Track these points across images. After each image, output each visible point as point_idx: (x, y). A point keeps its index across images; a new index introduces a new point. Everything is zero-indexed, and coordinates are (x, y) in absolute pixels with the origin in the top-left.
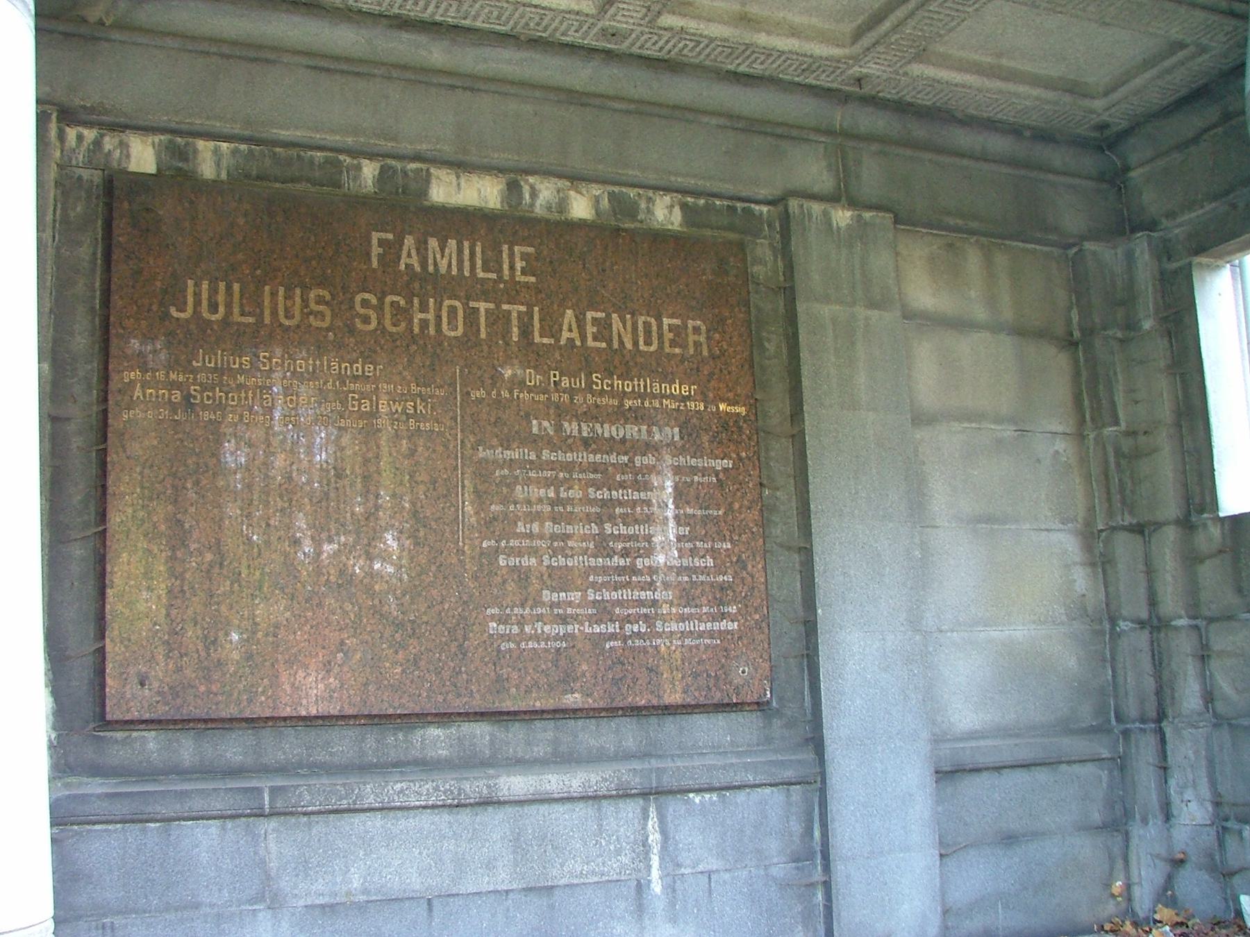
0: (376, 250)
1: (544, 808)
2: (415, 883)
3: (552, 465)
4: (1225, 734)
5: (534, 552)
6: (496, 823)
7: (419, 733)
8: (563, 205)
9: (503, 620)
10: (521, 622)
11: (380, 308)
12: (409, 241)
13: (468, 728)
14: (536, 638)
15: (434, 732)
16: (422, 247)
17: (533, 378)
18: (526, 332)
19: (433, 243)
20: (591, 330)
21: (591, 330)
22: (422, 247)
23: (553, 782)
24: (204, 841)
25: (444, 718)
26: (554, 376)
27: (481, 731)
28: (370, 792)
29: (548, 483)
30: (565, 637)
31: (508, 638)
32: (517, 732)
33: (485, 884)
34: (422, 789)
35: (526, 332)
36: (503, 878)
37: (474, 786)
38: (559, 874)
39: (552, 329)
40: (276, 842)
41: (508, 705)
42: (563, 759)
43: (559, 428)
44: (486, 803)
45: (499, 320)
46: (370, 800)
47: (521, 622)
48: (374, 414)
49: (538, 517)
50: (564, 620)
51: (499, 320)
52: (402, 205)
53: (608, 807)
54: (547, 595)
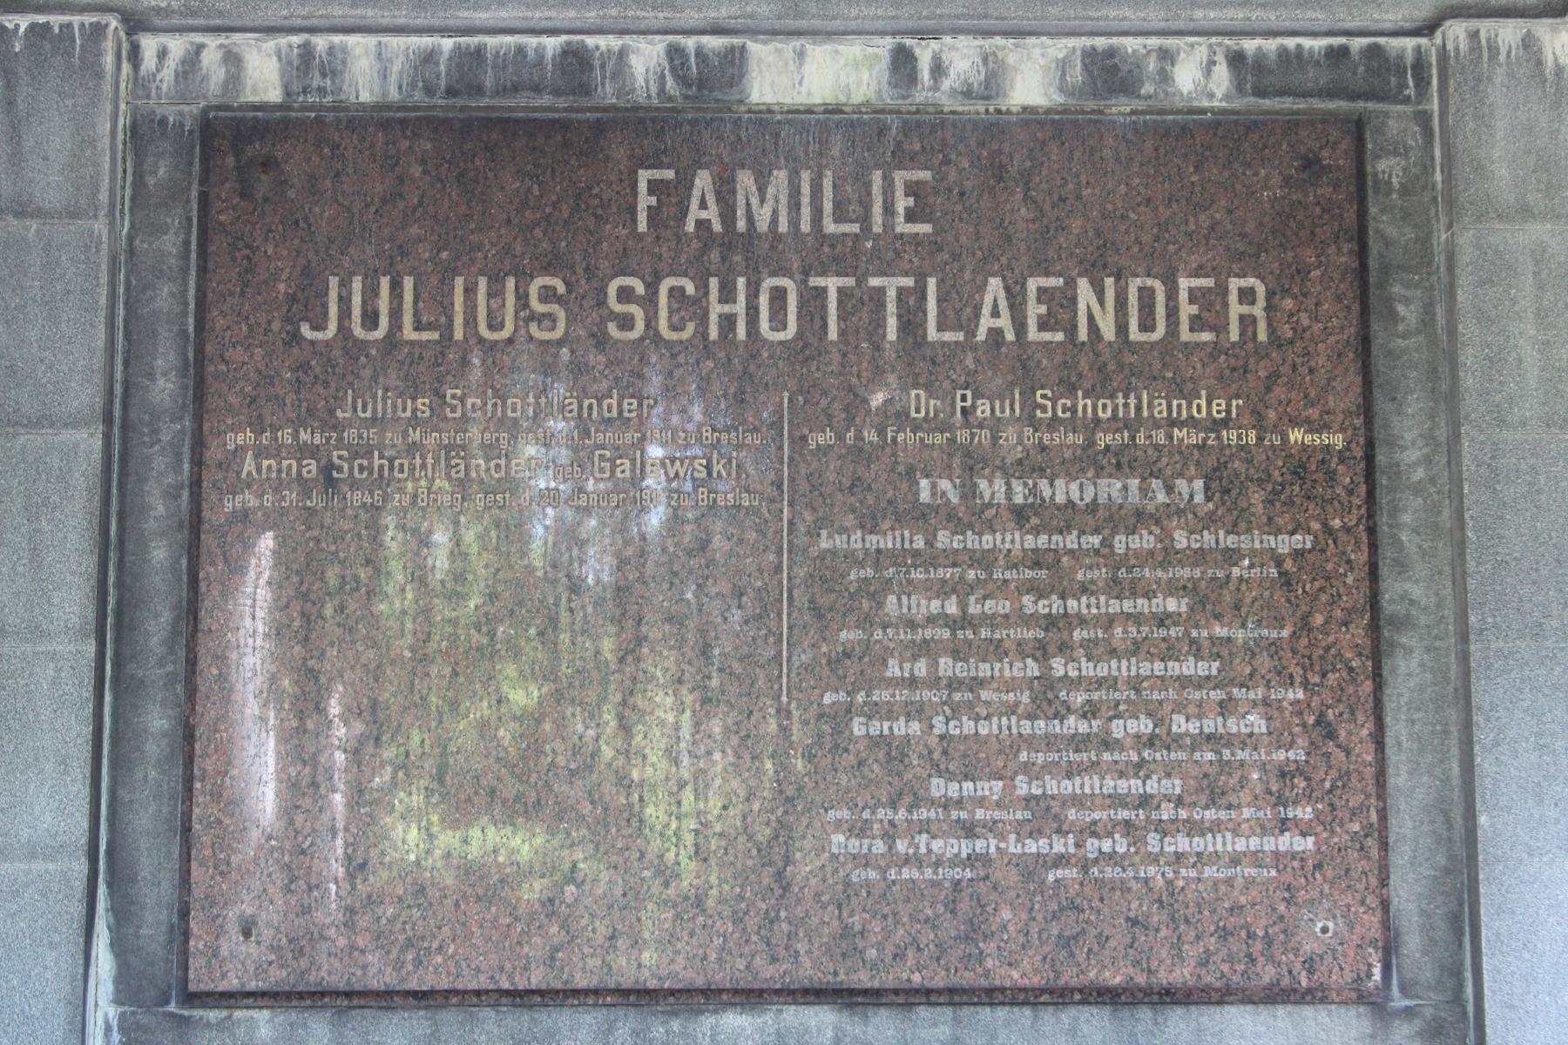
0: (645, 201)
3: (952, 558)
5: (916, 711)
8: (994, 79)
9: (860, 830)
10: (889, 836)
11: (650, 301)
12: (703, 181)
17: (921, 404)
18: (911, 323)
21: (1035, 310)
29: (943, 590)
31: (866, 861)
35: (911, 323)
39: (960, 313)
43: (969, 492)
47: (889, 836)
49: (925, 649)
50: (969, 830)
54: (938, 787)
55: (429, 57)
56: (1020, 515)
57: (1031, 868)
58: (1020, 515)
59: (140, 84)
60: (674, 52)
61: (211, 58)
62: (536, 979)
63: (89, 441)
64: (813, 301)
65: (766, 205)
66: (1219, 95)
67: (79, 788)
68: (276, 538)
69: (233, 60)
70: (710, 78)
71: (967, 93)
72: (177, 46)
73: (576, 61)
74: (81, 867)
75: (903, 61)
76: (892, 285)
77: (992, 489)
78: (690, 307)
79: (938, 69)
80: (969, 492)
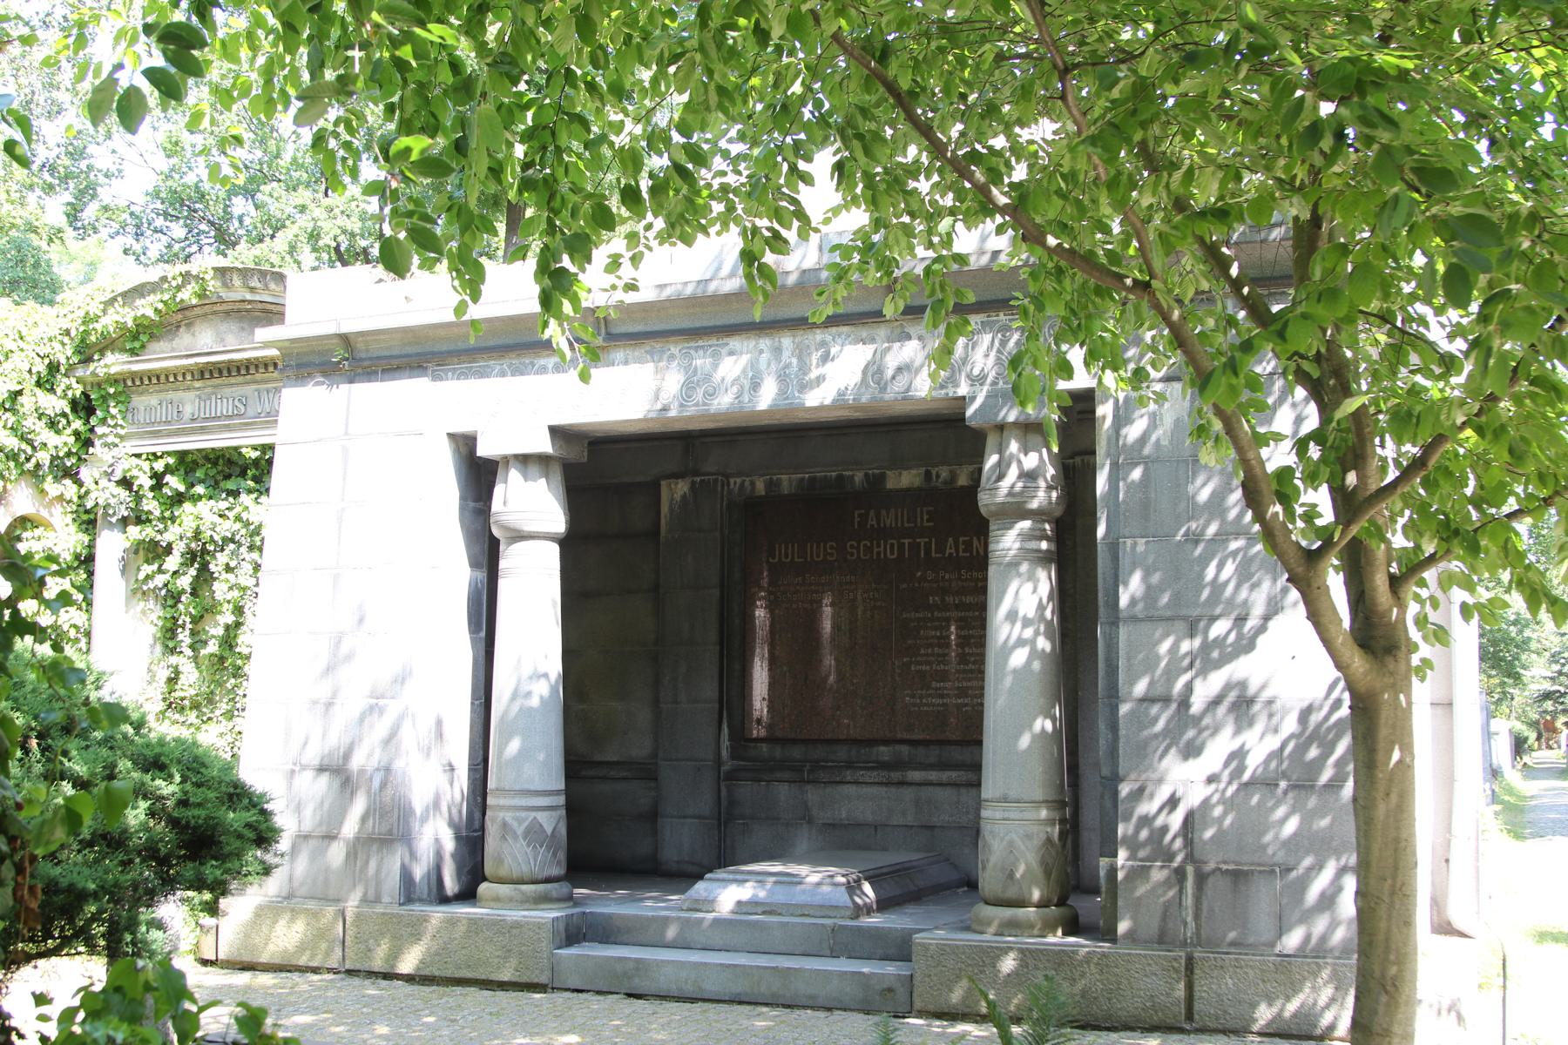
0: (857, 520)
1: (931, 789)
2: (869, 817)
3: (938, 619)
4: (483, 888)
5: (929, 663)
6: (908, 793)
7: (875, 750)
8: (953, 477)
9: (913, 696)
10: (921, 697)
11: (858, 548)
12: (872, 513)
13: (898, 747)
14: (928, 705)
15: (882, 748)
16: (878, 516)
17: (930, 575)
18: (928, 551)
19: (884, 512)
20: (961, 547)
21: (961, 547)
22: (878, 516)
23: (933, 776)
24: (783, 792)
25: (886, 742)
26: (942, 574)
27: (905, 750)
28: (849, 775)
29: (936, 629)
30: (943, 705)
31: (914, 705)
32: (921, 750)
33: (901, 821)
34: (873, 776)
35: (928, 551)
36: (910, 819)
37: (896, 776)
38: (935, 821)
39: (940, 549)
40: (813, 795)
41: (915, 737)
42: (943, 766)
43: (943, 600)
44: (902, 783)
45: (915, 547)
46: (849, 778)
47: (921, 697)
48: (855, 600)
49: (931, 645)
50: (942, 696)
51: (915, 547)
52: (875, 489)
53: (963, 790)
54: (934, 684)
55: (802, 480)
56: (957, 607)
57: (959, 707)
58: (957, 607)
59: (730, 492)
60: (866, 475)
61: (747, 484)
62: (830, 736)
63: (716, 592)
64: (901, 546)
65: (889, 520)
66: (101, 693)
67: (716, 684)
68: (1461, 544)
69: (753, 484)
70: (876, 482)
71: (945, 483)
72: (739, 480)
73: (840, 478)
74: (717, 706)
75: (928, 474)
76: (922, 541)
77: (949, 599)
78: (869, 550)
79: (938, 476)
80: (943, 600)
